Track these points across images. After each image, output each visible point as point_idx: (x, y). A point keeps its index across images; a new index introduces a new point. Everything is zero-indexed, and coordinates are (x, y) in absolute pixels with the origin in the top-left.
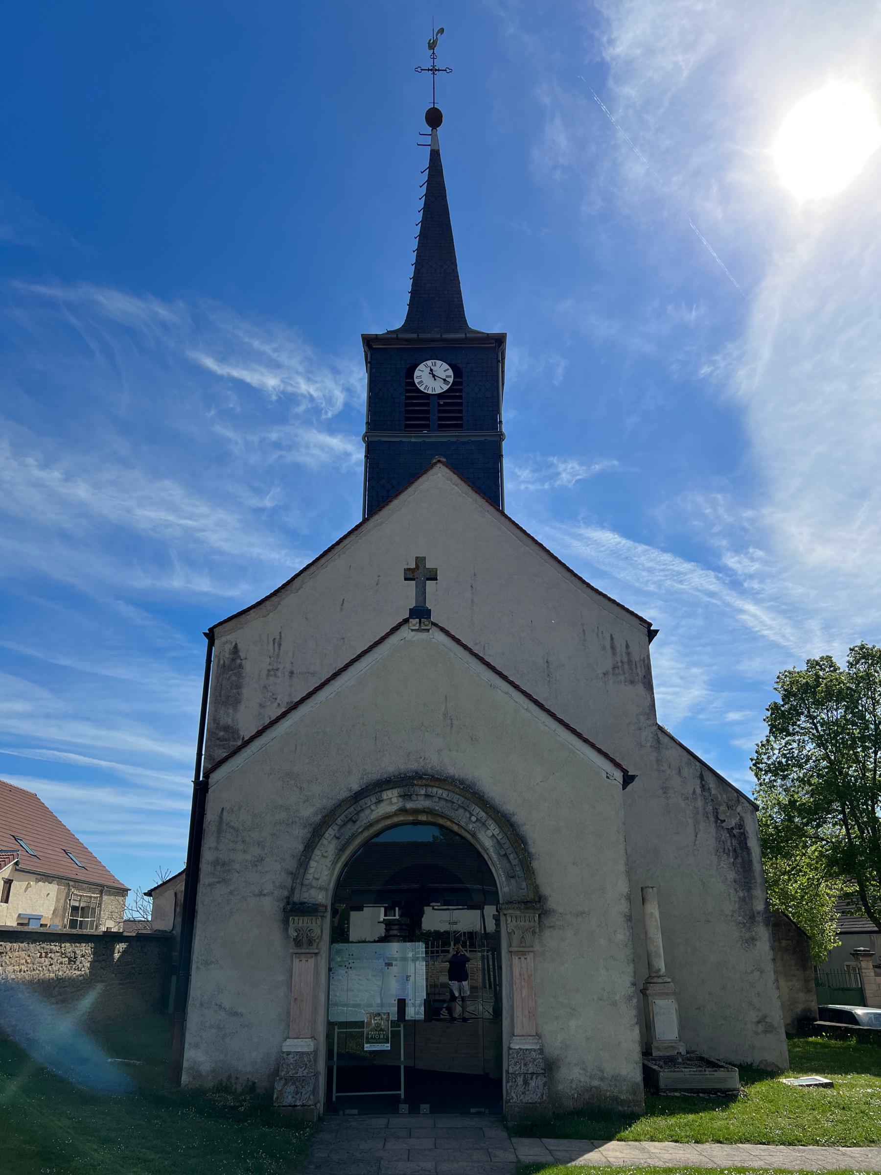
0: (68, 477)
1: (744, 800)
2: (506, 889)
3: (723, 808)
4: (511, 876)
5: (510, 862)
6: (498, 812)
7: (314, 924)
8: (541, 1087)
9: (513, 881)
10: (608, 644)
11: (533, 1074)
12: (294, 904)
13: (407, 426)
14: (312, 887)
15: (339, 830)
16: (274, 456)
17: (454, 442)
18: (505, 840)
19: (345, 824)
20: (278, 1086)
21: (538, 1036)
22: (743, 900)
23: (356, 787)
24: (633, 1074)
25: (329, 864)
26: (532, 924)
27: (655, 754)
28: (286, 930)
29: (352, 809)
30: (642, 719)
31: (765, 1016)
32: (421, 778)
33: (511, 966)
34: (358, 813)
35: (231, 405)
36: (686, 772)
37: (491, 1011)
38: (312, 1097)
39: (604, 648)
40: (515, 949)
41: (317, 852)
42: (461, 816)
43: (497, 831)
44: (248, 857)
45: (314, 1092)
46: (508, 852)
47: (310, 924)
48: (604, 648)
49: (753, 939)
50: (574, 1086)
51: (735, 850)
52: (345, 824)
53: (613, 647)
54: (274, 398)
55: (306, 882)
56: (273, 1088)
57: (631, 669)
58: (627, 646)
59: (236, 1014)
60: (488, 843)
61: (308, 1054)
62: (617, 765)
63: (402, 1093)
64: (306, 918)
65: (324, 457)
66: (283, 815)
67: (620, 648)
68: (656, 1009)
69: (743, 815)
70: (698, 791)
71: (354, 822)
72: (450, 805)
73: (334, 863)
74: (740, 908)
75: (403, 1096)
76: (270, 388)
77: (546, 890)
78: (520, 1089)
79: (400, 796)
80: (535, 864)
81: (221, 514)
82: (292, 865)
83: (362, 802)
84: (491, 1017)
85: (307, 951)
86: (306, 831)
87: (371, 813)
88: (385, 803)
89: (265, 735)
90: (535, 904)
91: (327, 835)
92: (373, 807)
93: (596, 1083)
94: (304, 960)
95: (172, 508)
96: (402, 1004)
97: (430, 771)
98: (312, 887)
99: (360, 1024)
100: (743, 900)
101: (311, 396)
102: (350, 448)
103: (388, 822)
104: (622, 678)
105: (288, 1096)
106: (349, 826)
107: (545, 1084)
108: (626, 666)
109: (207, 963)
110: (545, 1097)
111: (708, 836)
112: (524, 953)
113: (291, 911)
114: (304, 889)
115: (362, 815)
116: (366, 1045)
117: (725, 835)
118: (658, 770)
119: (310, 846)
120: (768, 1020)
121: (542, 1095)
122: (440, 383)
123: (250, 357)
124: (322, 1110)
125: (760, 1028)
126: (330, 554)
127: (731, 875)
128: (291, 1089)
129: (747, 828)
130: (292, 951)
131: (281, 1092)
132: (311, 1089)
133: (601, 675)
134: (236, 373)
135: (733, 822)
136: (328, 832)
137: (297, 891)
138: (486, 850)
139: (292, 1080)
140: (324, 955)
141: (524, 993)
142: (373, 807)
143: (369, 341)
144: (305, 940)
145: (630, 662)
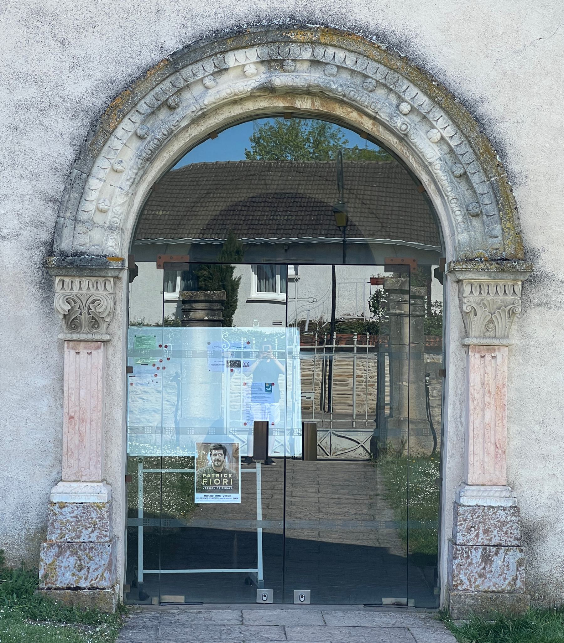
2: (463, 237)
4: (473, 214)
5: (472, 188)
6: (454, 96)
7: (101, 291)
8: (513, 566)
9: (476, 222)
11: (499, 546)
12: (64, 254)
14: (94, 225)
15: (143, 122)
18: (465, 148)
20: (47, 557)
21: (511, 486)
23: (173, 44)
25: (126, 185)
26: (509, 298)
28: (48, 299)
29: (166, 84)
32: (302, 27)
33: (466, 371)
34: (179, 92)
37: (368, 447)
38: (107, 575)
40: (476, 341)
42: (380, 103)
43: (450, 131)
45: (110, 566)
46: (470, 169)
47: (93, 290)
55: (84, 216)
56: (37, 560)
60: (432, 153)
61: (98, 507)
63: (260, 570)
64: (85, 280)
66: (30, 92)
71: (172, 108)
72: (358, 80)
73: (135, 183)
75: (261, 577)
77: (535, 240)
78: (476, 569)
79: (262, 62)
80: (519, 194)
82: (54, 185)
83: (187, 72)
84: (367, 457)
85: (90, 337)
86: (77, 123)
87: (203, 94)
88: (231, 74)
90: (515, 263)
91: (119, 132)
92: (208, 82)
94: (84, 353)
96: (261, 431)
97: (318, 15)
98: (94, 225)
99: (188, 461)
103: (237, 111)
105: (62, 572)
106: (163, 114)
107: (520, 563)
110: (519, 584)
112: (490, 348)
113: (58, 266)
114: (80, 228)
115: (187, 95)
116: (197, 495)
119: (87, 151)
121: (515, 580)
124: (121, 594)
130: (61, 336)
131: (52, 566)
132: (104, 562)
136: (122, 125)
137: (67, 232)
138: (426, 167)
139: (69, 547)
140: (119, 343)
141: (489, 415)
142: (208, 82)
144: (84, 317)
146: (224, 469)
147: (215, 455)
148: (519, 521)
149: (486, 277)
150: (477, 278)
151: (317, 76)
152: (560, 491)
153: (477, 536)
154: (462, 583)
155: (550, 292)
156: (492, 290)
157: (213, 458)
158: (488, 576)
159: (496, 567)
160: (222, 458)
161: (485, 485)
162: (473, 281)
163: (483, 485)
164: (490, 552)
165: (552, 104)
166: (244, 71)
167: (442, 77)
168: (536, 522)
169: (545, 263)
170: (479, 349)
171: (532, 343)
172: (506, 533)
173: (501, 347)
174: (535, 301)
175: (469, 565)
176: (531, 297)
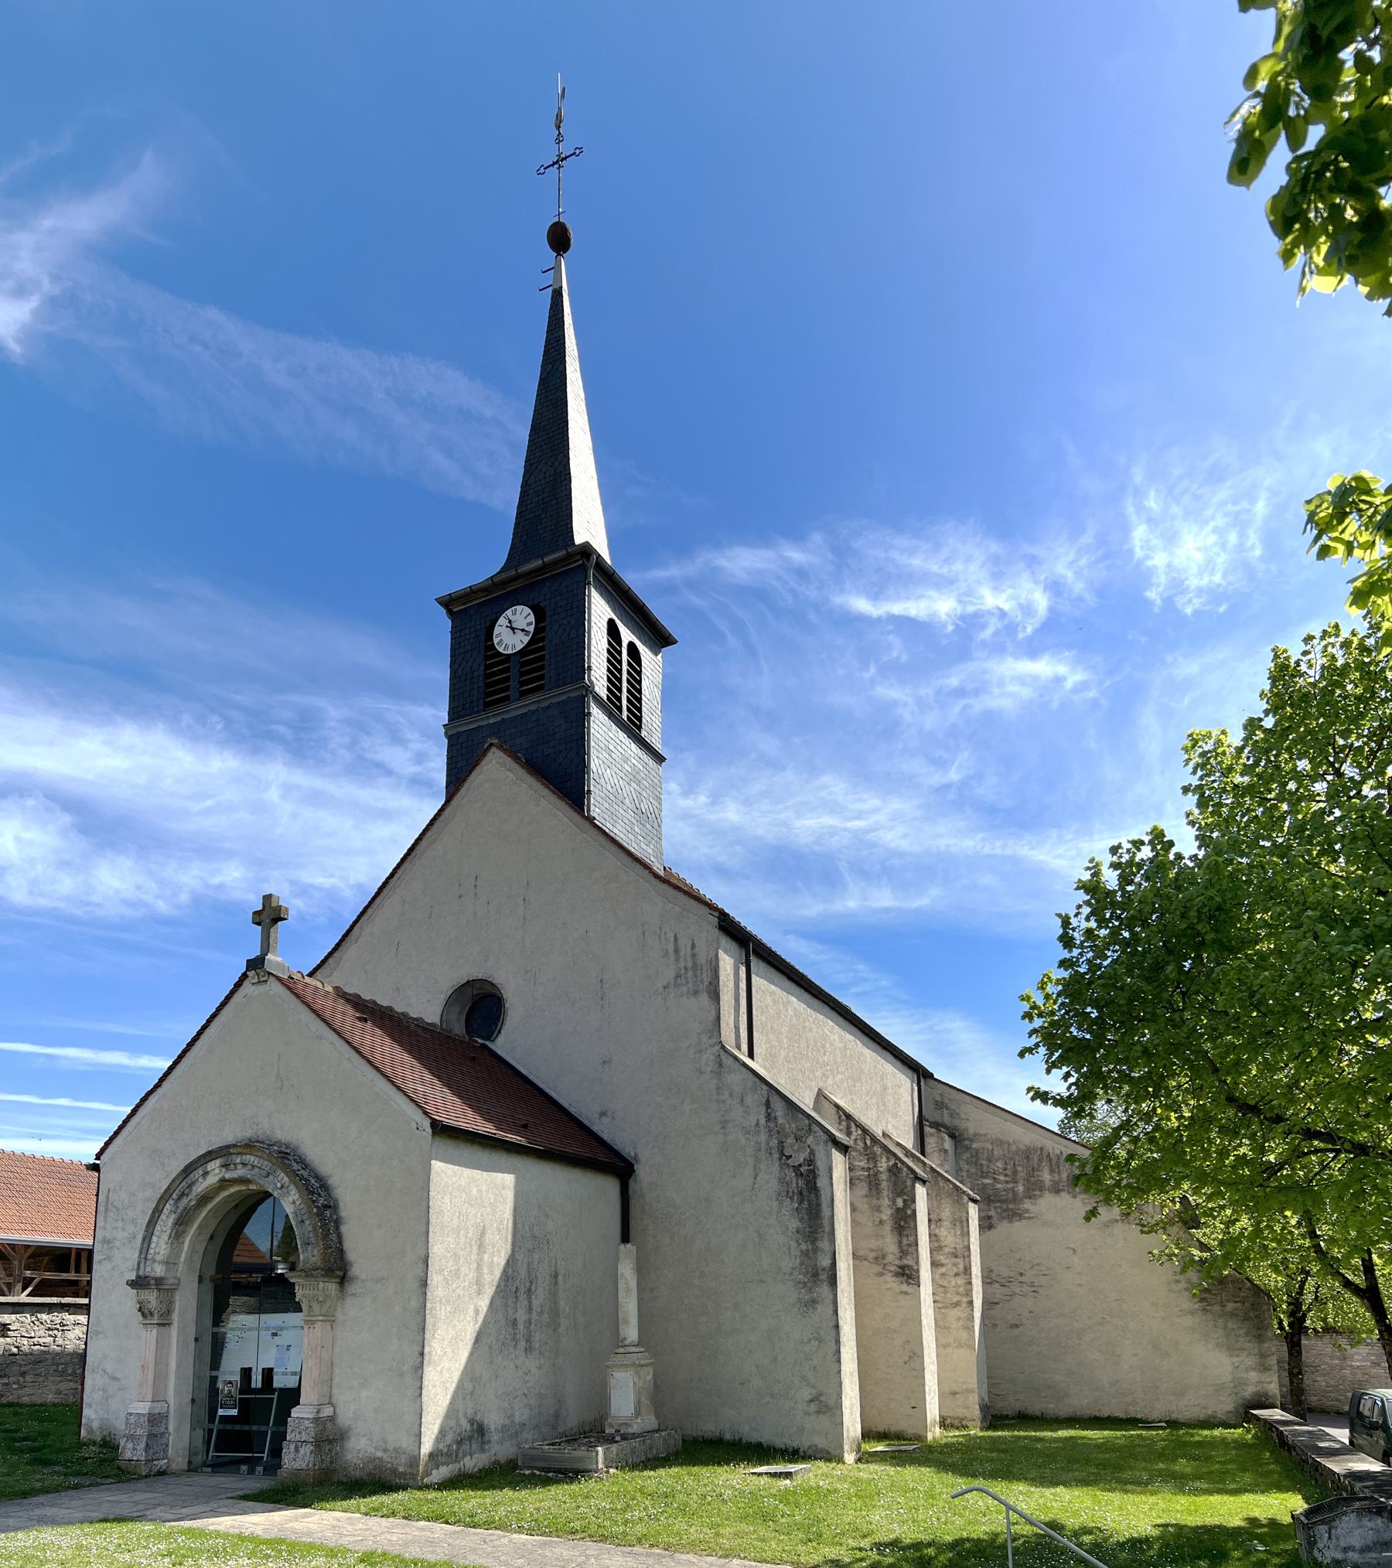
0: (716, 799)
1: (817, 1129)
3: (790, 1140)
10: (671, 948)
13: (487, 705)
16: (957, 709)
17: (533, 712)
19: (180, 1198)
22: (806, 1253)
27: (715, 1081)
30: (704, 1039)
31: (821, 1394)
34: (190, 1186)
35: (895, 654)
36: (749, 1100)
39: (666, 953)
41: (158, 1228)
44: (126, 1235)
48: (666, 953)
49: (814, 1301)
51: (801, 1193)
52: (180, 1198)
53: (676, 951)
54: (950, 628)
57: (695, 976)
58: (693, 946)
59: (115, 1379)
62: (426, 1113)
65: (1026, 692)
67: (685, 951)
68: (613, 1382)
69: (814, 1147)
70: (763, 1121)
74: (802, 1263)
76: (944, 617)
77: (351, 1255)
80: (344, 1229)
81: (896, 804)
93: (379, 1454)
95: (835, 808)
100: (806, 1253)
101: (1001, 610)
102: (1062, 669)
104: (685, 989)
108: (690, 973)
109: (97, 1333)
111: (770, 1177)
117: (791, 1174)
118: (717, 1101)
120: (823, 1399)
122: (520, 635)
123: (909, 581)
125: (813, 1407)
126: (385, 891)
127: (794, 1224)
128: (130, 1445)
129: (819, 1163)
133: (661, 990)
134: (897, 608)
135: (801, 1157)
143: (448, 603)
145: (695, 965)
166: (216, 1170)
169: (356, 1270)
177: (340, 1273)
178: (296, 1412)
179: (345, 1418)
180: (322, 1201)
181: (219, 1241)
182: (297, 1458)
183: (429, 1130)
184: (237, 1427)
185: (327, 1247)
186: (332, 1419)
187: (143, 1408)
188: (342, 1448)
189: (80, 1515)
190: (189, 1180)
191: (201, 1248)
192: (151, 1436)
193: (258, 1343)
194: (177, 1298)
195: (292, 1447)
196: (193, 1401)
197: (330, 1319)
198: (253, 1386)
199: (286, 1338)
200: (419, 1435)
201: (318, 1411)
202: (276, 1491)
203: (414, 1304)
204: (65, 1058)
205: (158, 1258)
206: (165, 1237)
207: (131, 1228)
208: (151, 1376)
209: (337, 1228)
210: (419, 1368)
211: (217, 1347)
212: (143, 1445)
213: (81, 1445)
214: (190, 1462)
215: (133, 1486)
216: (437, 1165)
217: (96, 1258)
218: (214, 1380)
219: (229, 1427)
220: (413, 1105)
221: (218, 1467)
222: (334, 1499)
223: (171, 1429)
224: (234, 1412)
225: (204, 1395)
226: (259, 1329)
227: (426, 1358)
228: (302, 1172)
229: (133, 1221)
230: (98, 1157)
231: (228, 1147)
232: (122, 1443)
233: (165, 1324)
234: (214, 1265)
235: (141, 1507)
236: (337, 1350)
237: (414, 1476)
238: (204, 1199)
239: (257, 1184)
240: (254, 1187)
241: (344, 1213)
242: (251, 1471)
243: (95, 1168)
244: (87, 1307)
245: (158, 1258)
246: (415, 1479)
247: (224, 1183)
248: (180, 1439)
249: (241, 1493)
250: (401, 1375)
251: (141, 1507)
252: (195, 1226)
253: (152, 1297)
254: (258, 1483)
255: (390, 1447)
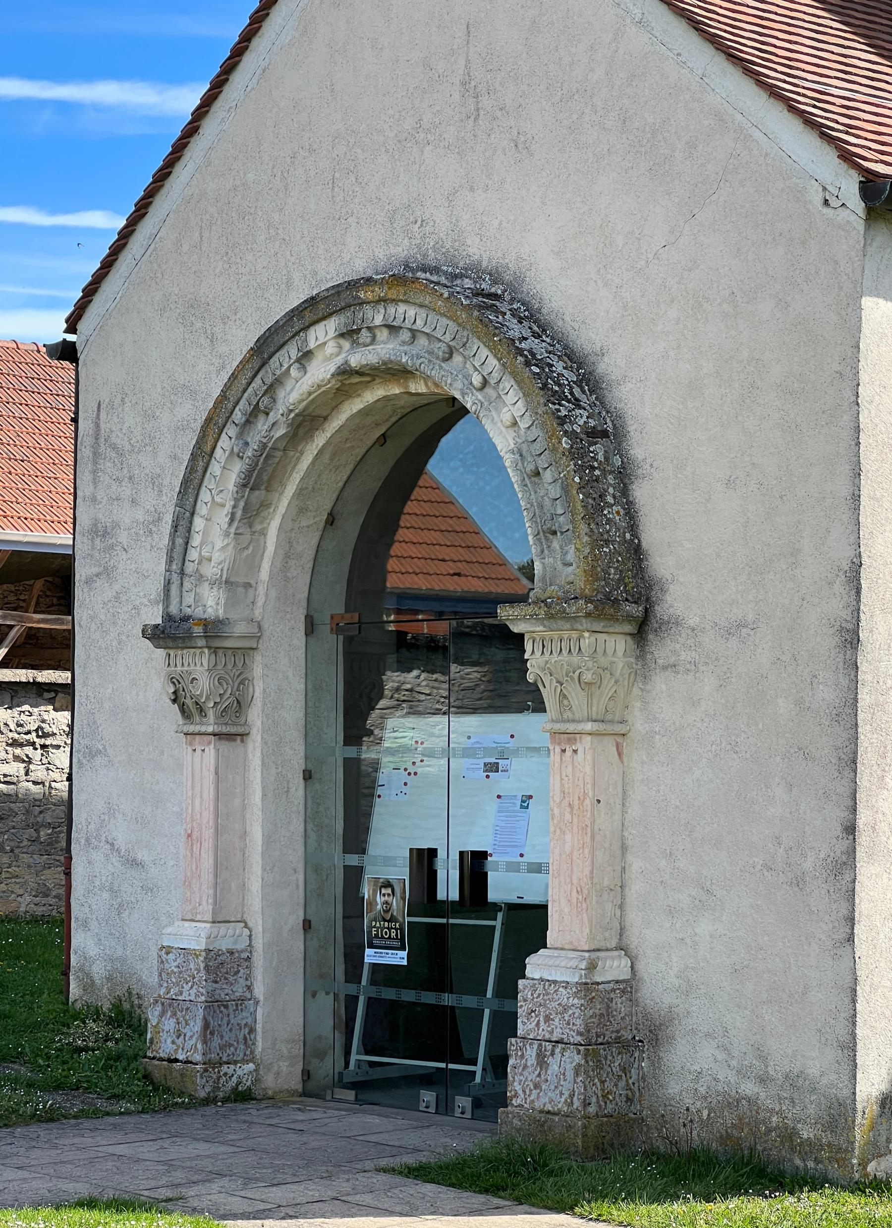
8: (570, 1074)
15: (240, 436)
19: (248, 422)
24: (833, 1077)
34: (271, 390)
41: (205, 496)
44: (140, 515)
50: (703, 1090)
52: (248, 422)
59: (134, 863)
62: (847, 157)
63: (478, 1069)
77: (662, 562)
79: (342, 335)
80: (640, 492)
83: (274, 362)
89: (152, 210)
93: (749, 1088)
109: (92, 754)
115: (281, 394)
116: (368, 951)
128: (169, 1024)
146: (392, 915)
147: (384, 895)
148: (582, 1005)
149: (541, 628)
150: (532, 629)
151: (391, 346)
152: (690, 966)
153: (538, 1025)
154: (516, 1095)
155: (678, 646)
156: (556, 646)
157: (383, 899)
158: (543, 1087)
159: (552, 1075)
160: (390, 899)
161: (230, 922)
162: (534, 635)
163: (562, 949)
164: (545, 1050)
165: (679, 347)
167: (560, 323)
168: (662, 1013)
170: (559, 739)
171: (657, 729)
172: (568, 1024)
173: (583, 736)
174: (660, 662)
175: (524, 1069)
176: (657, 656)
177: (636, 610)
178: (537, 966)
179: (661, 984)
180: (581, 418)
181: (351, 528)
182: (544, 1082)
183: (857, 205)
184: (408, 996)
185: (599, 541)
186: (628, 987)
187: (193, 936)
188: (656, 1063)
189: (41, 1186)
190: (267, 376)
191: (307, 546)
192: (215, 1004)
193: (450, 780)
194: (257, 670)
195: (531, 1053)
196: (307, 925)
197: (614, 731)
198: (441, 895)
199: (518, 776)
200: (850, 1047)
201: (592, 967)
202: (493, 1163)
203: (827, 694)
204: (97, 108)
205: (210, 571)
206: (222, 518)
207: (148, 499)
208: (207, 862)
209: (625, 491)
210: (844, 865)
211: (359, 794)
212: (196, 1026)
213: (69, 1015)
214: (307, 1075)
215: (171, 1122)
216: (867, 302)
217: (81, 572)
218: (353, 877)
219: (390, 994)
220: (811, 139)
221: (368, 1089)
222: (630, 1197)
223: (259, 990)
224: (400, 958)
225: (333, 910)
226: (448, 753)
227: (863, 839)
228: (531, 343)
229: (155, 481)
230: (72, 327)
231: (352, 285)
232: (153, 1016)
233: (232, 736)
234: (341, 588)
235: (179, 1176)
236: (634, 811)
237: (841, 1153)
238: (306, 422)
239: (427, 378)
240: (418, 387)
241: (639, 448)
242: (444, 1107)
243: (66, 352)
244: (68, 689)
245: (210, 571)
246: (844, 1162)
247: (349, 379)
248: (281, 1019)
249: (410, 1160)
250: (799, 882)
251: (179, 1176)
252: (290, 490)
253: (199, 667)
254: (453, 1137)
255: (778, 1067)
